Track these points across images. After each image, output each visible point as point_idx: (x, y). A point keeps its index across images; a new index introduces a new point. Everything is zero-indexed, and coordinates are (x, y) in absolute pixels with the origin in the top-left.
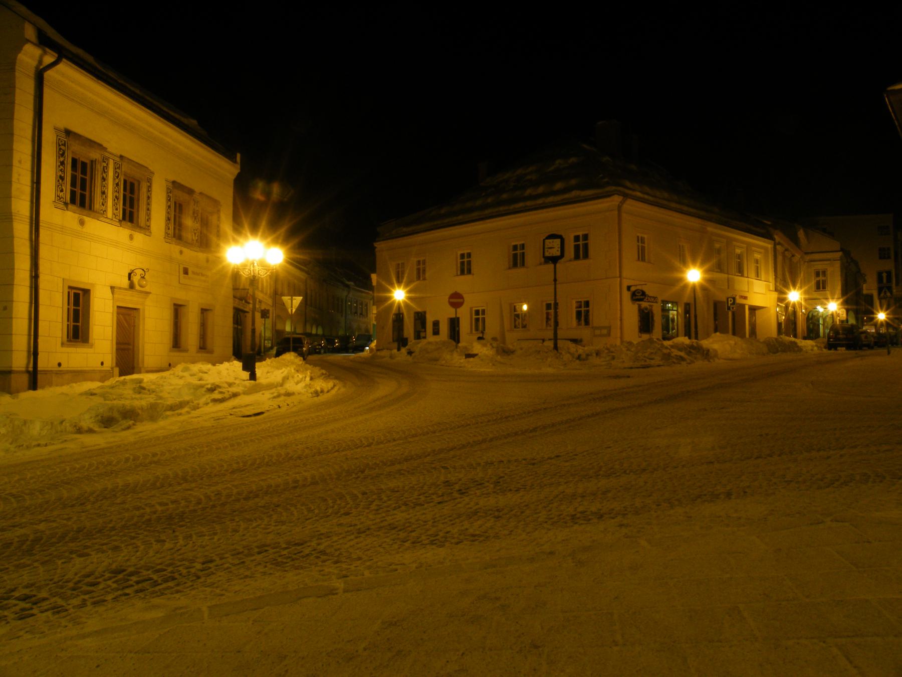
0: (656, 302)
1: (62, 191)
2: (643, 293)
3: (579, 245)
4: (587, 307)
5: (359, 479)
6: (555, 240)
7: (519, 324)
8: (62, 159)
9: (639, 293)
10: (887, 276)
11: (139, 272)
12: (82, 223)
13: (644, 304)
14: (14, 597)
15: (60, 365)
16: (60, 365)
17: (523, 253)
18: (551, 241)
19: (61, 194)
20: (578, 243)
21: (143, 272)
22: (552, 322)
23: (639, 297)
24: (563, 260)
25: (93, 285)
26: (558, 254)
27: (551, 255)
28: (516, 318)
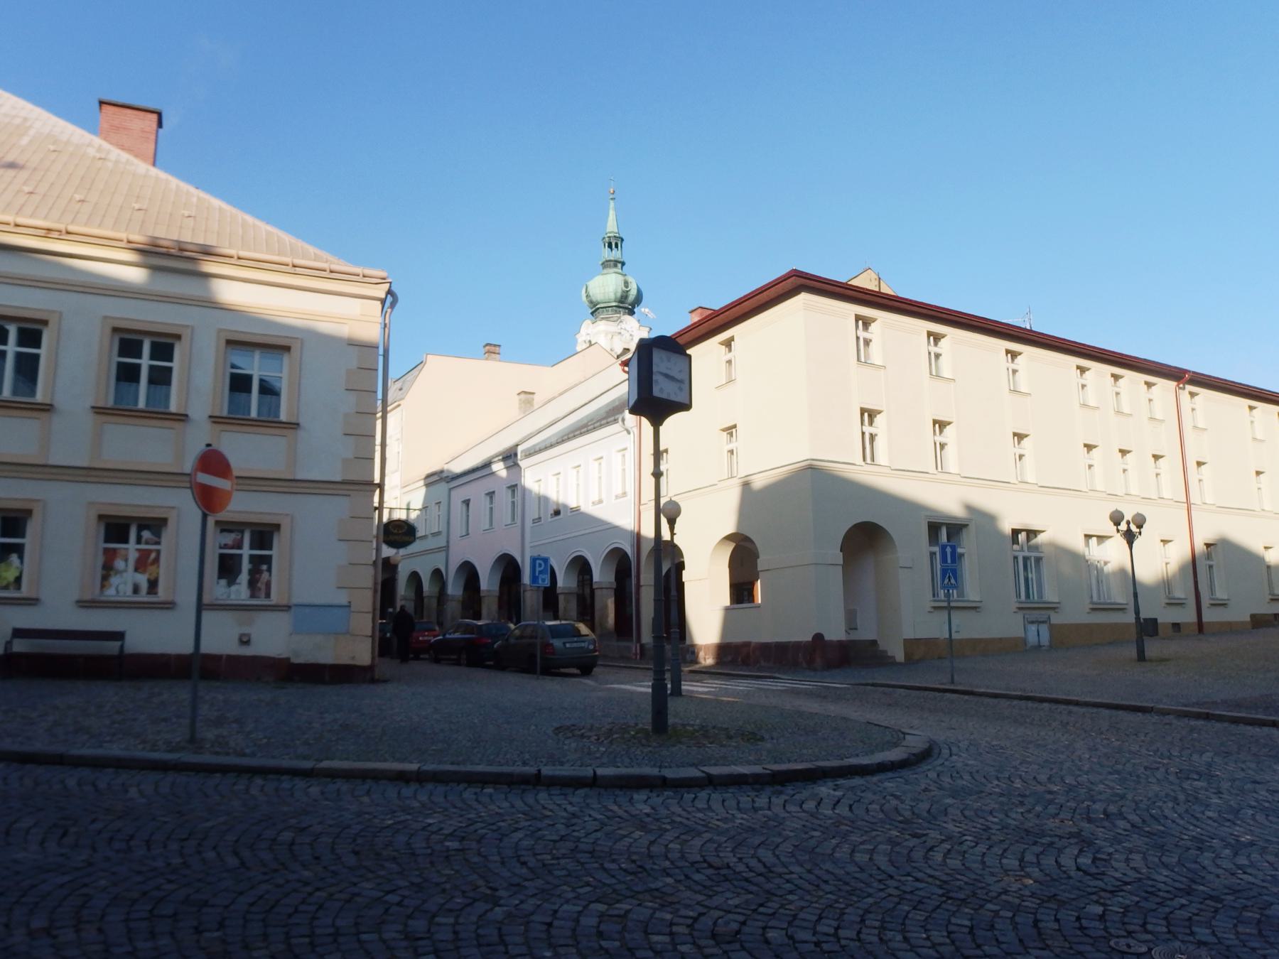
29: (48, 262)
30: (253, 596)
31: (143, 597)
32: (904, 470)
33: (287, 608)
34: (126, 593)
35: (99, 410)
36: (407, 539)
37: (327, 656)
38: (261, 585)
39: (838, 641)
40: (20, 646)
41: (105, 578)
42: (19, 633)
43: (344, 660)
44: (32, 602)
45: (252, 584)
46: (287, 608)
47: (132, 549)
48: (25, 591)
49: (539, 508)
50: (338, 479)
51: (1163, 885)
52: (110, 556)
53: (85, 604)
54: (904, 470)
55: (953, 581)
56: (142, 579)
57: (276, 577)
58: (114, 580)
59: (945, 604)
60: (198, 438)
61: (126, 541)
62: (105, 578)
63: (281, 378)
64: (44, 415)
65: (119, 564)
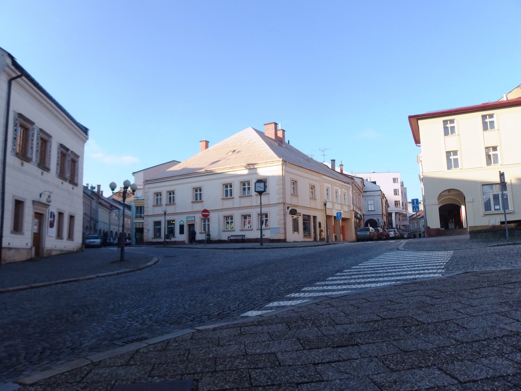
0: (300, 216)
1: (15, 145)
2: (296, 211)
3: (171, 197)
4: (266, 218)
5: (23, 357)
6: (261, 183)
7: (229, 227)
8: (15, 128)
9: (293, 210)
10: (416, 202)
11: (47, 194)
12: (22, 164)
13: (295, 217)
14: (153, 321)
15: (9, 244)
16: (9, 244)
17: (161, 198)
18: (259, 183)
19: (14, 147)
20: (227, 189)
21: (49, 193)
22: (403, 193)
23: (293, 213)
24: (265, 193)
25: (25, 199)
26: (263, 190)
27: (259, 190)
28: (227, 224)
29: (227, 174)
30: (266, 227)
31: (250, 229)
32: (519, 164)
33: (270, 229)
34: (247, 229)
35: (223, 199)
36: (295, 213)
37: (276, 238)
38: (267, 225)
39: (436, 229)
40: (232, 238)
41: (244, 226)
42: (232, 236)
43: (278, 238)
44: (234, 231)
45: (265, 225)
46: (270, 229)
47: (247, 220)
48: (233, 229)
49: (353, 201)
50: (277, 203)
51: (437, 297)
52: (245, 222)
53: (241, 230)
54: (519, 164)
55: (417, 210)
56: (249, 225)
57: (268, 223)
58: (245, 226)
59: (503, 212)
60: (164, 207)
61: (246, 219)
62: (244, 226)
63: (497, 154)
64: (202, 203)
65: (246, 223)
